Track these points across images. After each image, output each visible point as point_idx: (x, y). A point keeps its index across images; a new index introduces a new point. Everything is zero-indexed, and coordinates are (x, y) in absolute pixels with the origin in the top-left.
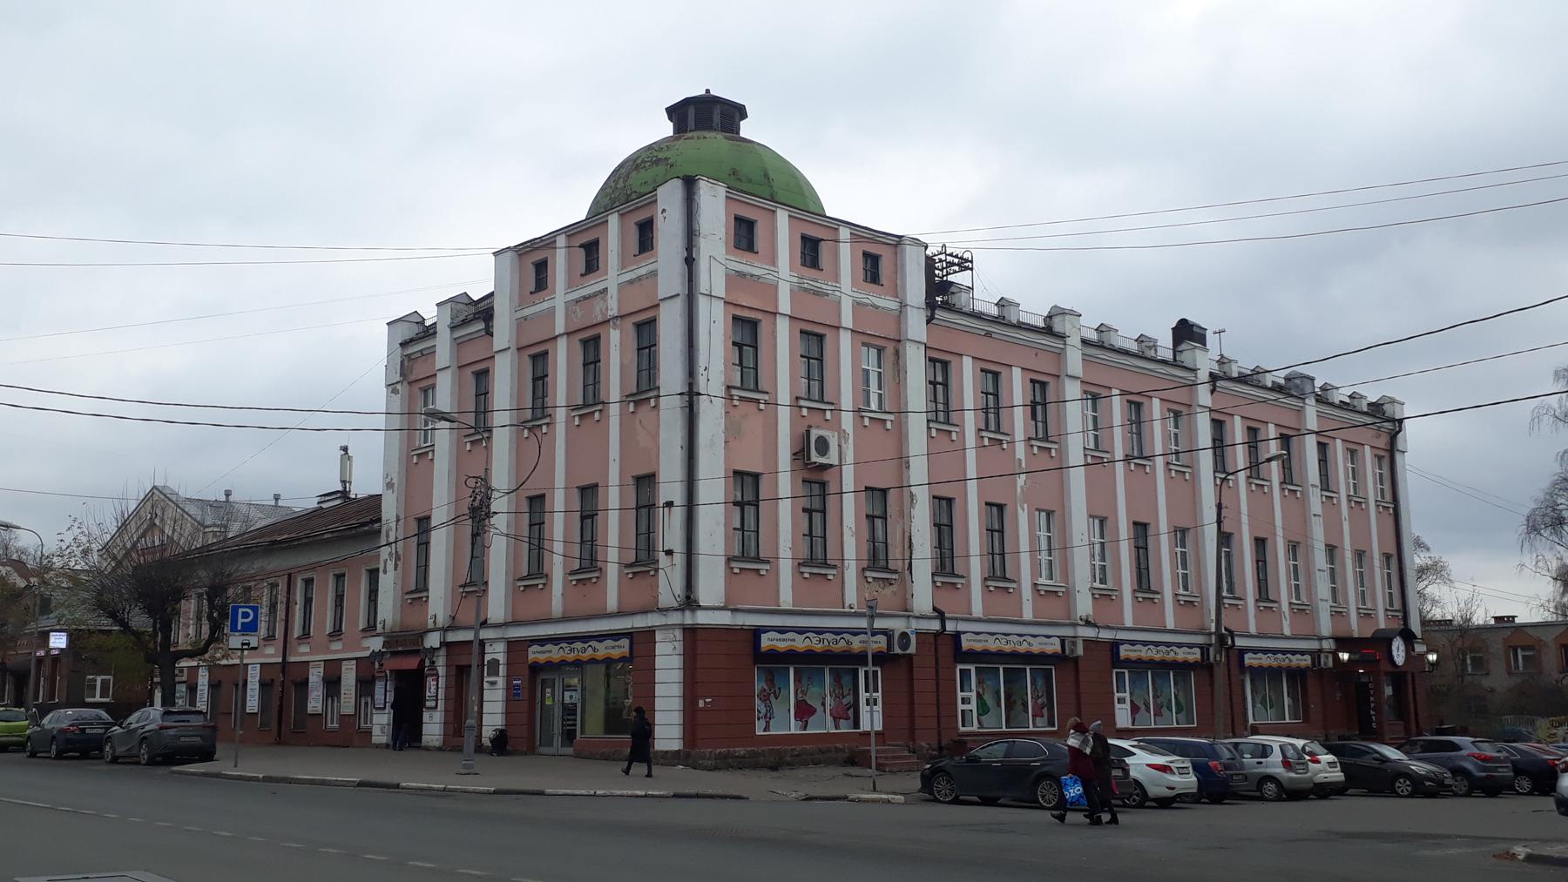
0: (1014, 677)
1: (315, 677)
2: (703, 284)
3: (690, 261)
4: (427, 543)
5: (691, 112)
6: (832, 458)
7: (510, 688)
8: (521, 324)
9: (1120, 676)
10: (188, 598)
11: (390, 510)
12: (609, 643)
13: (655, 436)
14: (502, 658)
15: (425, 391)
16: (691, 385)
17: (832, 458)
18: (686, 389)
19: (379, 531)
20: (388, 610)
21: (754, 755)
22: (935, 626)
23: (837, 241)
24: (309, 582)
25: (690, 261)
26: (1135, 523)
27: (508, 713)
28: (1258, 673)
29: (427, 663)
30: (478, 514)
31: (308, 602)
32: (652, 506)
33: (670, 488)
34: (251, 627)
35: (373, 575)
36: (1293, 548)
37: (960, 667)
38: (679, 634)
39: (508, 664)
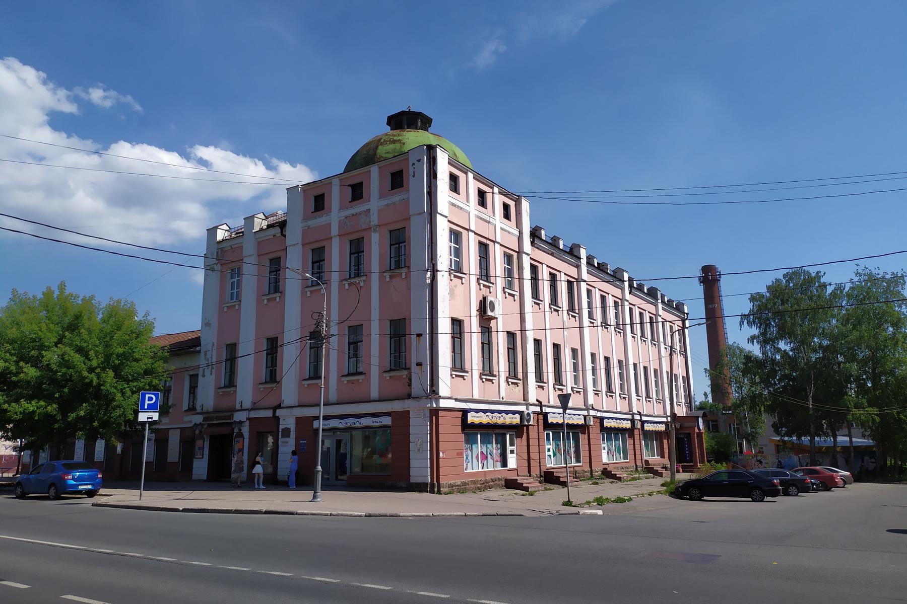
8: (306, 232)
11: (210, 341)
12: (510, 415)
19: (199, 352)
20: (207, 397)
21: (465, 484)
22: (538, 409)
29: (236, 430)
30: (316, 338)
35: (194, 378)
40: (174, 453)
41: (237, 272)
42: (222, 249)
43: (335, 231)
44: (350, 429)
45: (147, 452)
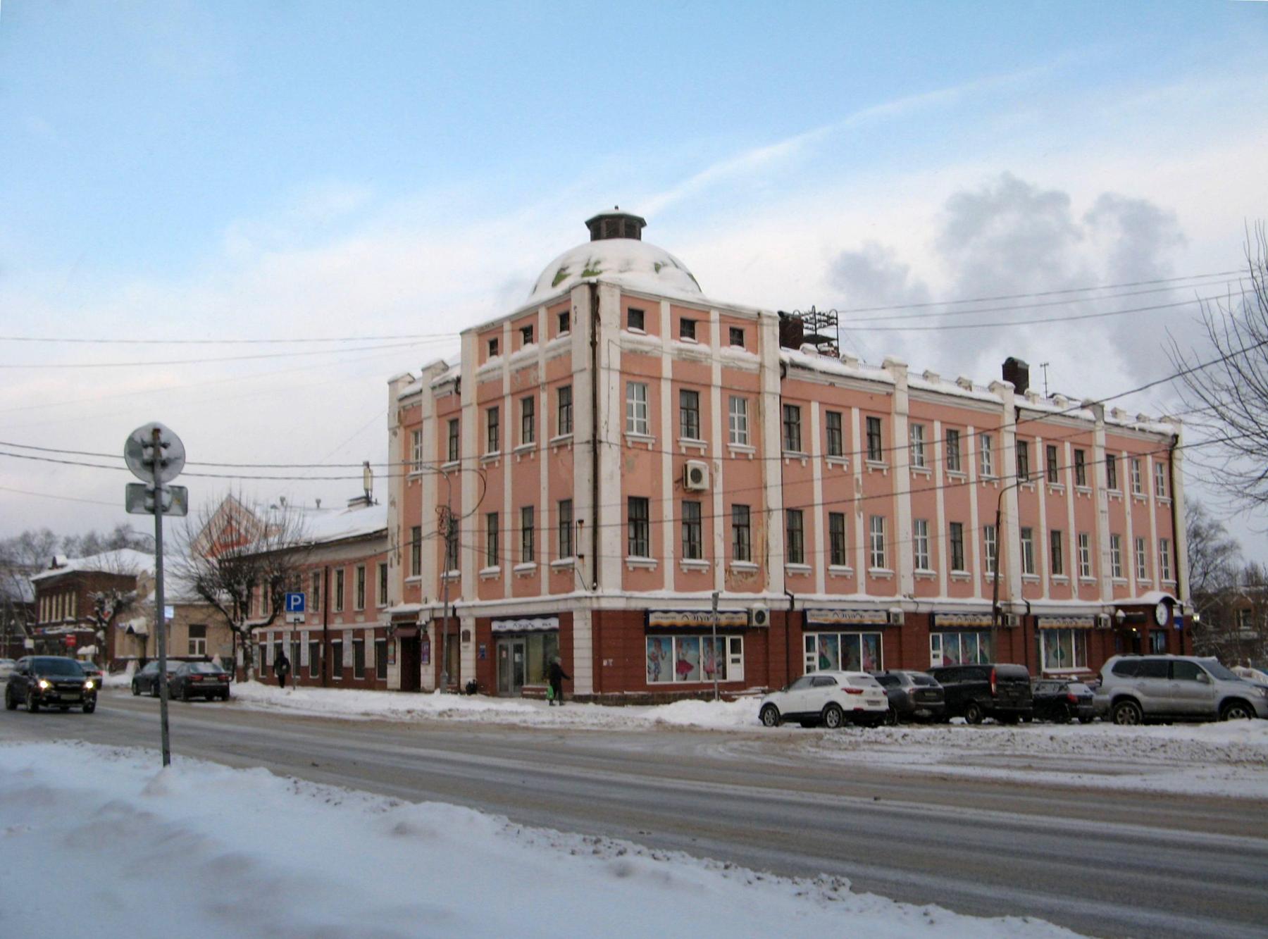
0: (849, 642)
1: (347, 641)
2: (603, 360)
3: (594, 344)
4: (420, 546)
5: (603, 225)
6: (705, 484)
7: (478, 650)
9: (935, 639)
10: (257, 586)
13: (571, 471)
14: (472, 630)
15: (416, 434)
16: (594, 436)
17: (705, 484)
18: (591, 438)
23: (708, 321)
24: (340, 573)
25: (594, 344)
26: (952, 524)
27: (478, 668)
28: (1050, 633)
31: (340, 586)
32: (569, 523)
33: (582, 510)
34: (300, 608)
35: (384, 568)
36: (1082, 540)
37: (805, 635)
38: (589, 615)
39: (477, 633)
40: (370, 661)
41: (418, 434)
42: (404, 408)
43: (506, 389)
44: (523, 633)
45: (348, 659)
